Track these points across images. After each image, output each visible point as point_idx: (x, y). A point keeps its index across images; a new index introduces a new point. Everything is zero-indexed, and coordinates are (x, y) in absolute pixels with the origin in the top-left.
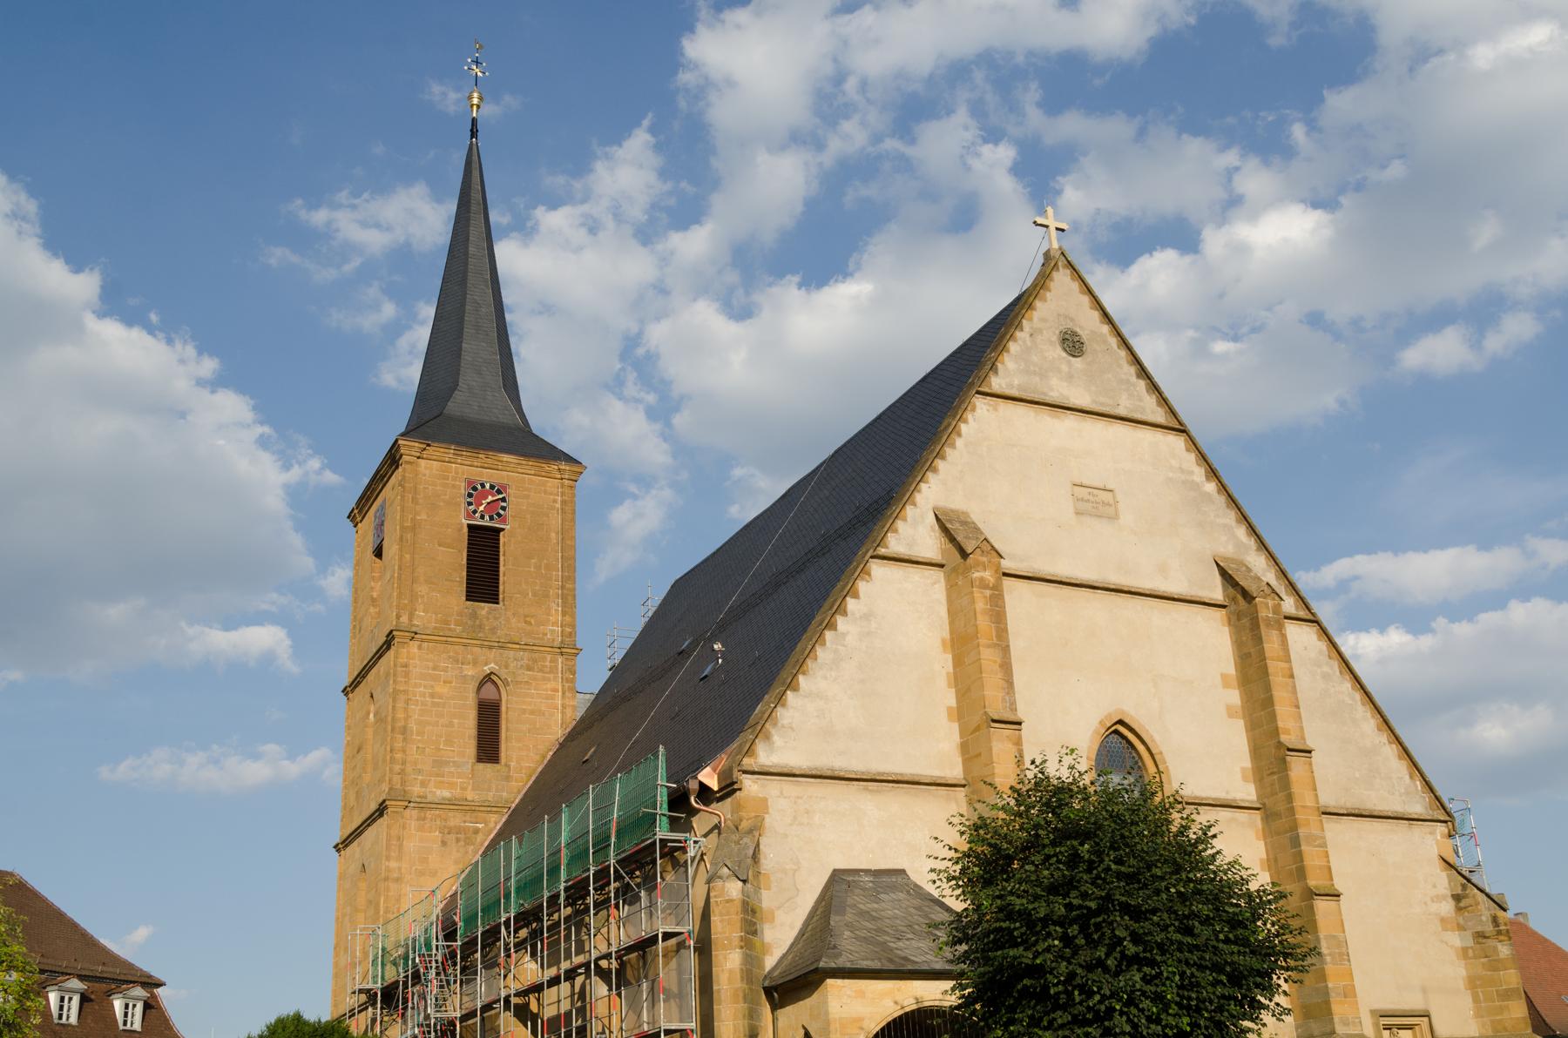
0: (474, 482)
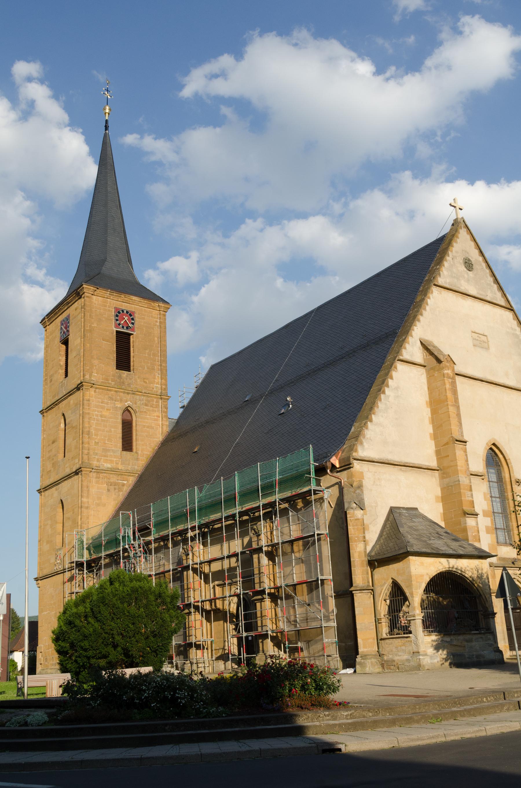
0: (119, 309)
